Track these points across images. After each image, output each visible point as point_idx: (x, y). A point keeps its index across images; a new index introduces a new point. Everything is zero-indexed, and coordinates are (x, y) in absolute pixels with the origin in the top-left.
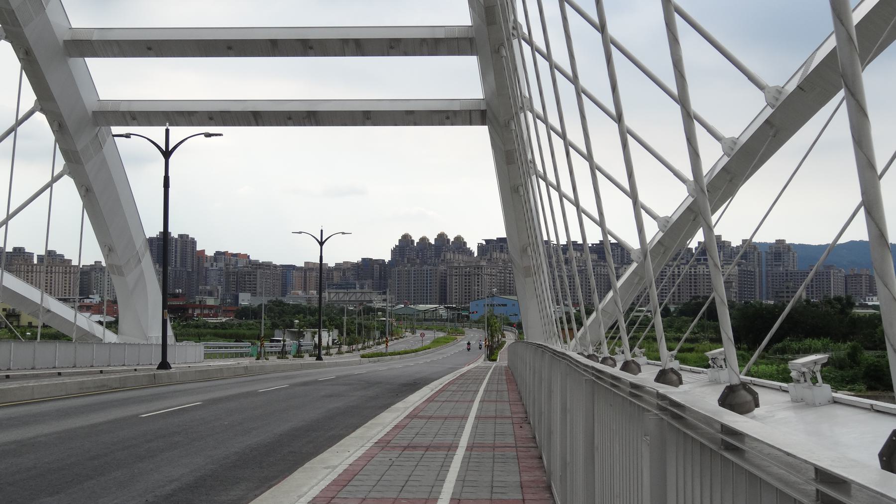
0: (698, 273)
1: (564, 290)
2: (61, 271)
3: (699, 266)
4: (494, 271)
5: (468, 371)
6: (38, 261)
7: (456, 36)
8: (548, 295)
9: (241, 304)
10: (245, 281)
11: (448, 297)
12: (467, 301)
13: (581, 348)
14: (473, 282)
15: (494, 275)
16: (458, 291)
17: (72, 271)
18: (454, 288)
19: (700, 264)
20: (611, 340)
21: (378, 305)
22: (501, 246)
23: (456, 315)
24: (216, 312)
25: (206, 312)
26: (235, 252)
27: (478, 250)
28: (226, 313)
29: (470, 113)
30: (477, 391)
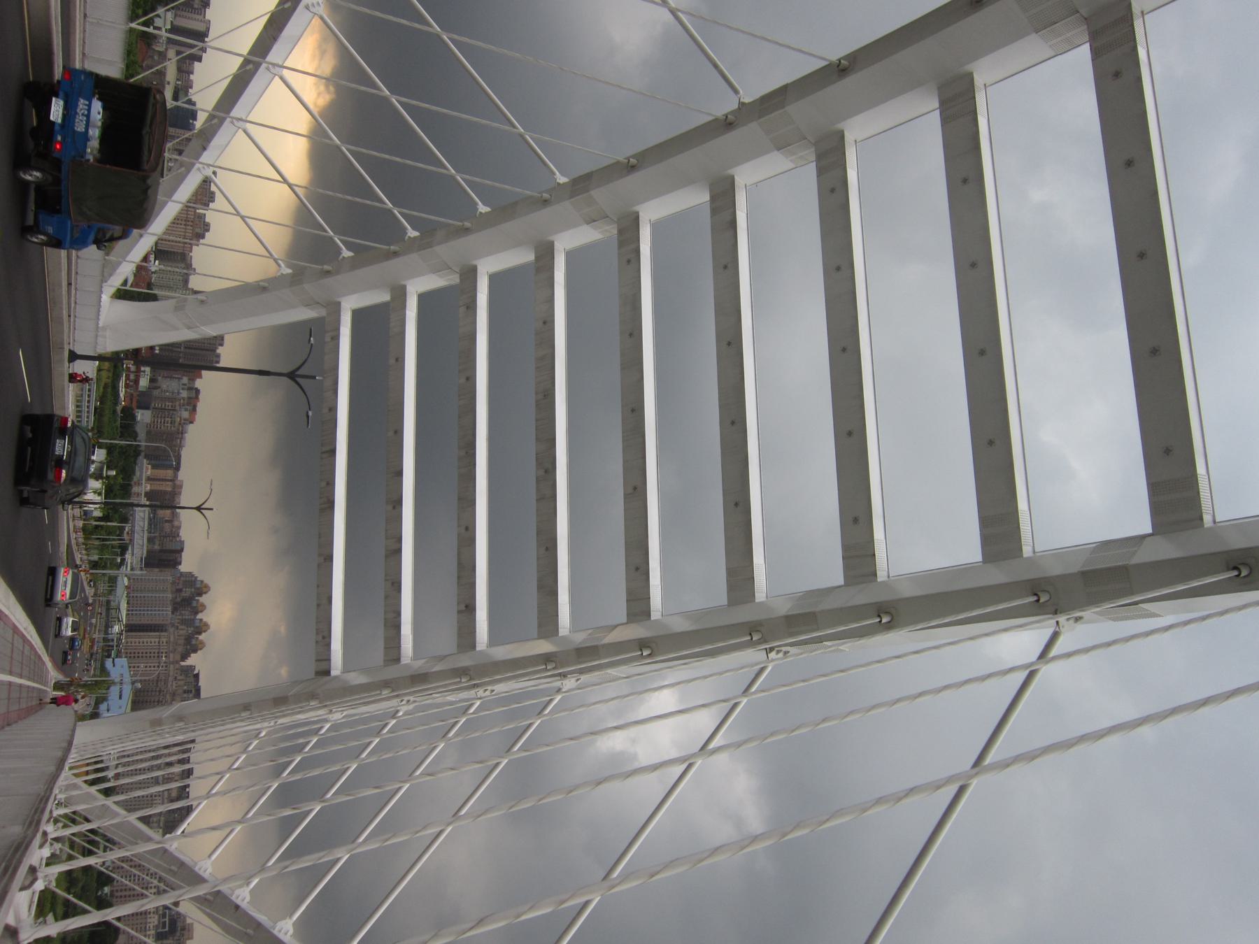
0: (149, 916)
1: (125, 774)
2: (187, 234)
3: (157, 917)
4: (163, 683)
5: (44, 663)
6: (199, 213)
7: (402, 646)
8: (130, 746)
9: (138, 412)
10: (164, 417)
11: (134, 634)
12: (129, 655)
13: (63, 786)
14: (151, 661)
15: (157, 683)
16: (141, 644)
17: (186, 245)
18: (145, 640)
19: (159, 918)
20: (159, 297)
21: (128, 556)
22: (191, 691)
23: (111, 644)
24: (131, 386)
25: (132, 377)
26: (197, 409)
27: (187, 666)
28: (129, 397)
29: (325, 660)
30: (21, 676)
